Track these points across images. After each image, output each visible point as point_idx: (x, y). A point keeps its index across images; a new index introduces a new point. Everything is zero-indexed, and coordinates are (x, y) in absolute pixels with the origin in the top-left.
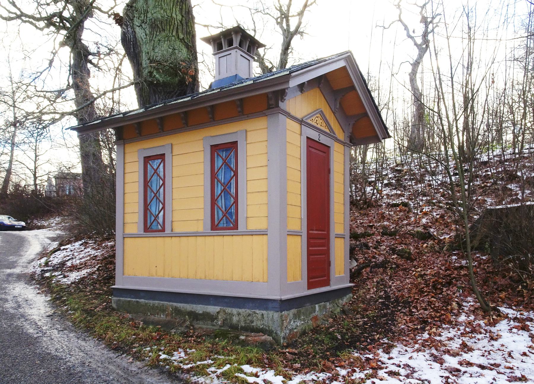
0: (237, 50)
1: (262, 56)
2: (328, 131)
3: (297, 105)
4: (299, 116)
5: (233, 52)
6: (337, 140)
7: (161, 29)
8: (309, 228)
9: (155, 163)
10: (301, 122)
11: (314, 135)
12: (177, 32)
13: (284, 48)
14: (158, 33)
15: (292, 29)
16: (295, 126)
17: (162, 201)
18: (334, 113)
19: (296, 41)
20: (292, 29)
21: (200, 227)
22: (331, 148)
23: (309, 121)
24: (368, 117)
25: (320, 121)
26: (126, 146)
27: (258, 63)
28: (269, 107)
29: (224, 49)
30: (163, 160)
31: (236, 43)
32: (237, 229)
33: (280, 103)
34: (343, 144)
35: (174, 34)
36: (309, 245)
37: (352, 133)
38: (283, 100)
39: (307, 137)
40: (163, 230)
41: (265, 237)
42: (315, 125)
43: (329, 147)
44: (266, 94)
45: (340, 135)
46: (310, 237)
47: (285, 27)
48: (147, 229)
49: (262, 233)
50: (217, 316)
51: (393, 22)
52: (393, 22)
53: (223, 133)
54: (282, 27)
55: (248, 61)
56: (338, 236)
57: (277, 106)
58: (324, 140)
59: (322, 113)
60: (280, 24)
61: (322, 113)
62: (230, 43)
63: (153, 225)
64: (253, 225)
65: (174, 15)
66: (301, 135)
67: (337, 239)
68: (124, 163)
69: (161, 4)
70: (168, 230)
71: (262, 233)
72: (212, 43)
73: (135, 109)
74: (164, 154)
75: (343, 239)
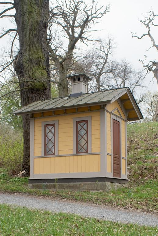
0: (82, 82)
2: (119, 116)
3: (109, 108)
4: (110, 111)
7: (36, 64)
9: (50, 128)
10: (111, 113)
11: (115, 118)
12: (43, 65)
13: (70, 47)
15: (76, 35)
16: (109, 115)
17: (53, 142)
18: (121, 109)
19: (78, 44)
20: (76, 35)
21: (71, 153)
22: (121, 123)
25: (117, 112)
28: (101, 109)
31: (82, 79)
32: (88, 152)
34: (125, 121)
35: (42, 66)
36: (114, 160)
37: (128, 116)
40: (54, 154)
41: (99, 155)
42: (115, 114)
43: (120, 122)
45: (123, 117)
47: (71, 33)
48: (46, 153)
49: (98, 154)
50: (80, 186)
51: (144, 35)
52: (144, 35)
54: (68, 34)
55: (85, 86)
58: (118, 119)
60: (67, 31)
61: (117, 110)
62: (79, 79)
63: (48, 152)
64: (94, 151)
65: (42, 58)
66: (111, 118)
69: (36, 52)
70: (56, 154)
71: (98, 154)
72: (71, 79)
74: (55, 124)
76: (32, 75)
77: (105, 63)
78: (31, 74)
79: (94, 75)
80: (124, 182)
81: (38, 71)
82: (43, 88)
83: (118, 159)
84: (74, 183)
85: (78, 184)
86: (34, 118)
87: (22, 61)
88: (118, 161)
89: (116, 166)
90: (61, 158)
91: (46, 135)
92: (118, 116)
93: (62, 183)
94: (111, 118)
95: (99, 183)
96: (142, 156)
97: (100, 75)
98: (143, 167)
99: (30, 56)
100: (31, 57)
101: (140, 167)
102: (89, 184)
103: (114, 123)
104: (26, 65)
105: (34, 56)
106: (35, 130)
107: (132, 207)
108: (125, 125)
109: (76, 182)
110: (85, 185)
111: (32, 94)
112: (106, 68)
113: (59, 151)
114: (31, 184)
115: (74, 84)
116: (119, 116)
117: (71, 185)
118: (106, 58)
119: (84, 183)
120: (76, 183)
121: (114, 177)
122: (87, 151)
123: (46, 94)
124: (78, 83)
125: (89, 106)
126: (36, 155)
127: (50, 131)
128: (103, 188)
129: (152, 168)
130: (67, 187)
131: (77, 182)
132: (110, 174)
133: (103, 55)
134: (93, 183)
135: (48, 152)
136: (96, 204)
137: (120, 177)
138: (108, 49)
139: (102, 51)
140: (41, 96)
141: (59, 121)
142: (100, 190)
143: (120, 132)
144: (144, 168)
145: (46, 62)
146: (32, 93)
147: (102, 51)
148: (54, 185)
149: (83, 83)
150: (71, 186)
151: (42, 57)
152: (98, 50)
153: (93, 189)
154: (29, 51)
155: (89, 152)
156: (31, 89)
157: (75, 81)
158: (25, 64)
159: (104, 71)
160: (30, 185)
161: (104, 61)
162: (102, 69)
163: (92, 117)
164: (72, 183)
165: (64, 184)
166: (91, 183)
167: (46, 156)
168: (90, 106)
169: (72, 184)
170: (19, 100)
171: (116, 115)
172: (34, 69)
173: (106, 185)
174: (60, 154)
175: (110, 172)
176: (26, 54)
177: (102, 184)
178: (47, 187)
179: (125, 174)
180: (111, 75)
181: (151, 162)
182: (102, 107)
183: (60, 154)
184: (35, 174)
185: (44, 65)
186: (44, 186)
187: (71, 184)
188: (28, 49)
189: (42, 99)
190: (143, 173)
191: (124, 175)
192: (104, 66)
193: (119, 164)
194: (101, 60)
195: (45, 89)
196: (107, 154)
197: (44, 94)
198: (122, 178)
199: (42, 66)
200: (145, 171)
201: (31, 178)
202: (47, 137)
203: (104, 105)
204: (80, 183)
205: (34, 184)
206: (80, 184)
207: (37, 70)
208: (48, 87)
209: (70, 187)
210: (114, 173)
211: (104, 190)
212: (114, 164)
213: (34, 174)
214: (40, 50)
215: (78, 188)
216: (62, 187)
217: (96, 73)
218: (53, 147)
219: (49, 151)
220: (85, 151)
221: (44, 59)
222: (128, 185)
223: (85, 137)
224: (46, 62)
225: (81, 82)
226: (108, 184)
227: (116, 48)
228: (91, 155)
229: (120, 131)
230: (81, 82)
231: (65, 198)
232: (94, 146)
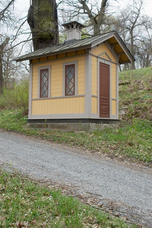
1: (90, 10)
2: (109, 59)
3: (93, 52)
4: (96, 55)
5: (73, 30)
6: (112, 62)
8: (100, 95)
10: (97, 57)
11: (103, 61)
14: (43, 18)
16: (96, 58)
18: (111, 53)
22: (110, 66)
23: (101, 57)
24: (125, 53)
25: (105, 56)
26: (33, 66)
27: (88, 15)
28: (86, 53)
29: (70, 29)
30: (48, 71)
31: (75, 27)
32: (74, 95)
33: (89, 51)
34: (116, 64)
35: (50, 18)
36: (100, 101)
38: (90, 50)
39: (100, 62)
41: (84, 97)
44: (85, 49)
45: (113, 60)
46: (100, 99)
49: (83, 96)
53: (69, 61)
56: (113, 100)
57: (88, 52)
58: (107, 63)
59: (106, 53)
61: (106, 53)
62: (73, 27)
64: (80, 93)
65: (49, 10)
66: (97, 61)
67: (112, 101)
68: (33, 72)
71: (83, 96)
73: (114, 98)
75: (115, 101)
76: (41, 26)
77: (137, 17)
78: (40, 25)
79: (129, 28)
80: (116, 122)
81: (46, 23)
82: (50, 37)
83: (107, 100)
84: (63, 123)
85: (65, 124)
86: (32, 64)
87: (33, 14)
88: (107, 102)
89: (104, 107)
90: (53, 100)
91: (41, 80)
92: (108, 60)
93: (53, 123)
94: (97, 61)
95: (83, 124)
96: (141, 96)
97: (133, 27)
98: (138, 107)
99: (39, 9)
100: (40, 10)
101: (135, 107)
102: (74, 125)
103: (102, 66)
104: (36, 18)
105: (43, 9)
106: (33, 75)
107: (99, 151)
108: (116, 68)
109: (64, 123)
110: (71, 125)
111: (41, 43)
112: (139, 21)
113: (78, 91)
114: (29, 124)
115: (69, 31)
116: (109, 59)
117: (60, 125)
118: (138, 13)
119: (70, 123)
120: (64, 123)
121: (100, 117)
122: (74, 94)
123: (53, 43)
124: (72, 30)
125: (75, 50)
126: (34, 97)
127: (45, 75)
128: (87, 129)
129: (146, 108)
130: (56, 127)
131: (66, 122)
132: (96, 115)
133: (136, 11)
134: (78, 123)
135: (43, 94)
136: (68, 146)
137: (109, 117)
138: (140, 5)
139: (135, 8)
140: (49, 45)
141: (52, 66)
142: (84, 131)
143: (109, 75)
144: (139, 108)
145: (53, 14)
146: (41, 42)
147: (135, 8)
148: (46, 124)
149: (76, 30)
150: (60, 127)
151: (50, 10)
152: (132, 6)
153: (77, 130)
154: (39, 4)
155: (76, 94)
156: (40, 38)
157: (69, 28)
158: (35, 16)
159: (136, 24)
160: (28, 124)
161: (137, 16)
162: (135, 22)
163: (78, 61)
164: (61, 123)
165: (55, 124)
166: (76, 123)
167: (41, 99)
168: (77, 50)
169: (61, 124)
170: (148, 57)
171: (104, 59)
172: (42, 21)
173: (89, 127)
174: (79, 95)
175: (96, 113)
176: (36, 8)
177: (86, 125)
178: (40, 127)
179: (115, 114)
180: (143, 27)
181: (147, 102)
182: (87, 51)
183: (52, 96)
184: (32, 114)
185: (52, 17)
186: (39, 125)
187: (60, 124)
188: (37, 3)
189: (50, 46)
190: (137, 112)
191: (114, 114)
192: (136, 20)
193: (108, 106)
194: (134, 15)
195: (52, 38)
196: (91, 96)
197: (51, 43)
198: (111, 118)
199: (50, 18)
200: (139, 111)
201: (30, 117)
202: (43, 82)
203: (88, 49)
204: (67, 123)
205: (31, 123)
206: (67, 125)
207: (45, 22)
208: (55, 37)
209: (59, 127)
210: (100, 113)
211: (87, 132)
212: (101, 105)
213: (31, 114)
214: (48, 3)
215: (65, 128)
216: (53, 127)
217: (130, 27)
218: (47, 90)
219: (43, 94)
220: (72, 94)
221: (52, 11)
222: (119, 124)
223: (73, 79)
224: (53, 14)
225: (74, 30)
226: (93, 125)
227: (147, 3)
228: (67, 98)
229: (109, 74)
230: (74, 29)
231: (46, 139)
232: (80, 88)
